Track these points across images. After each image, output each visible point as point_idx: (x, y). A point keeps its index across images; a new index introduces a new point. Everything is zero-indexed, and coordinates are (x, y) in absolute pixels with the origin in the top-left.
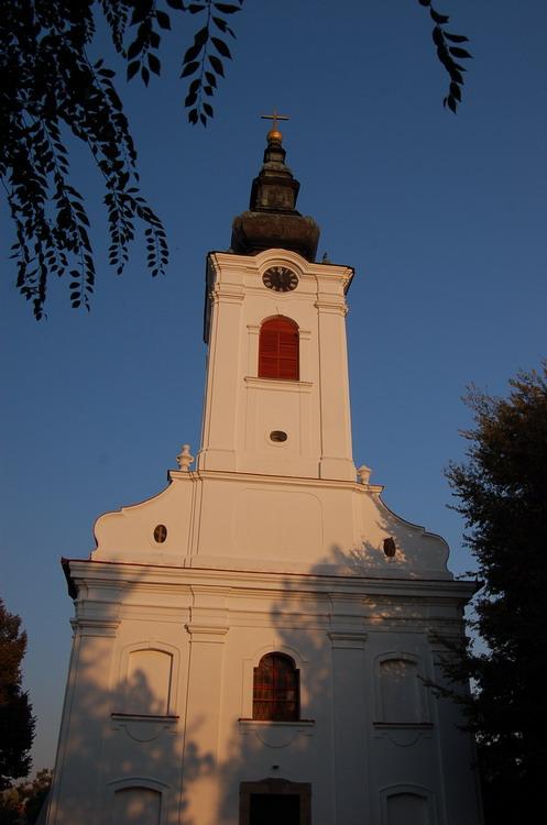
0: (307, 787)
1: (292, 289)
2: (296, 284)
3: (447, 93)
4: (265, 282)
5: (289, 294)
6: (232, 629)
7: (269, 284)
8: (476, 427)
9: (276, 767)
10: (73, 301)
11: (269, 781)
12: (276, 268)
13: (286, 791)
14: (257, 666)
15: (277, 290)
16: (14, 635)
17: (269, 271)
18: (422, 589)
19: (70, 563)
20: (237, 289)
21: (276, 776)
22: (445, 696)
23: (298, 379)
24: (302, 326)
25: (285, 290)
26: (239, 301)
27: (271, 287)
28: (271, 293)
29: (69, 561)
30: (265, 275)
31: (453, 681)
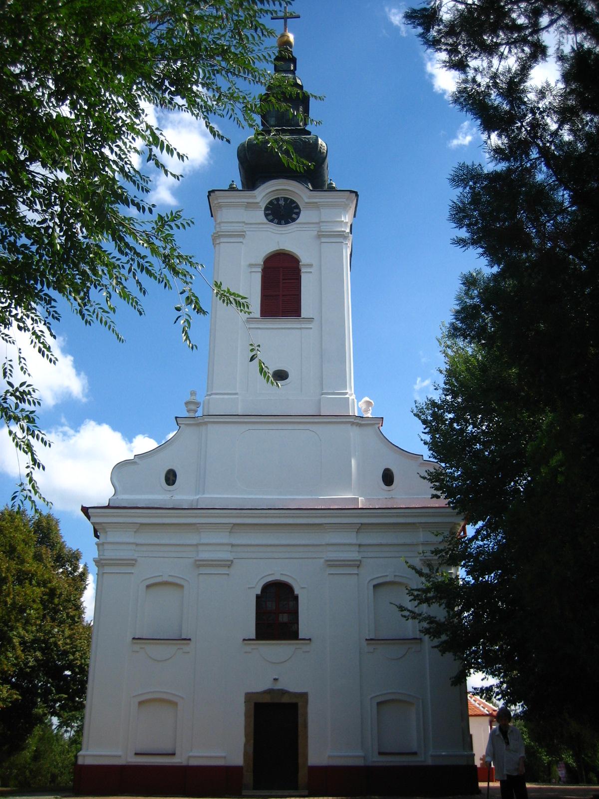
0: (304, 696)
1: (294, 220)
2: (298, 214)
3: (19, 362)
4: (266, 215)
5: (292, 227)
6: (234, 561)
7: (271, 217)
8: (444, 367)
9: (276, 680)
10: (145, 191)
11: (270, 692)
12: (277, 199)
13: (285, 700)
14: (259, 592)
15: (279, 223)
16: (75, 568)
17: (271, 203)
18: (406, 516)
19: (90, 510)
20: (237, 228)
21: (278, 686)
22: (414, 618)
23: (300, 316)
24: (304, 259)
25: (287, 223)
26: (241, 240)
27: (272, 221)
28: (274, 228)
29: (88, 508)
30: (266, 209)
31: (419, 604)
